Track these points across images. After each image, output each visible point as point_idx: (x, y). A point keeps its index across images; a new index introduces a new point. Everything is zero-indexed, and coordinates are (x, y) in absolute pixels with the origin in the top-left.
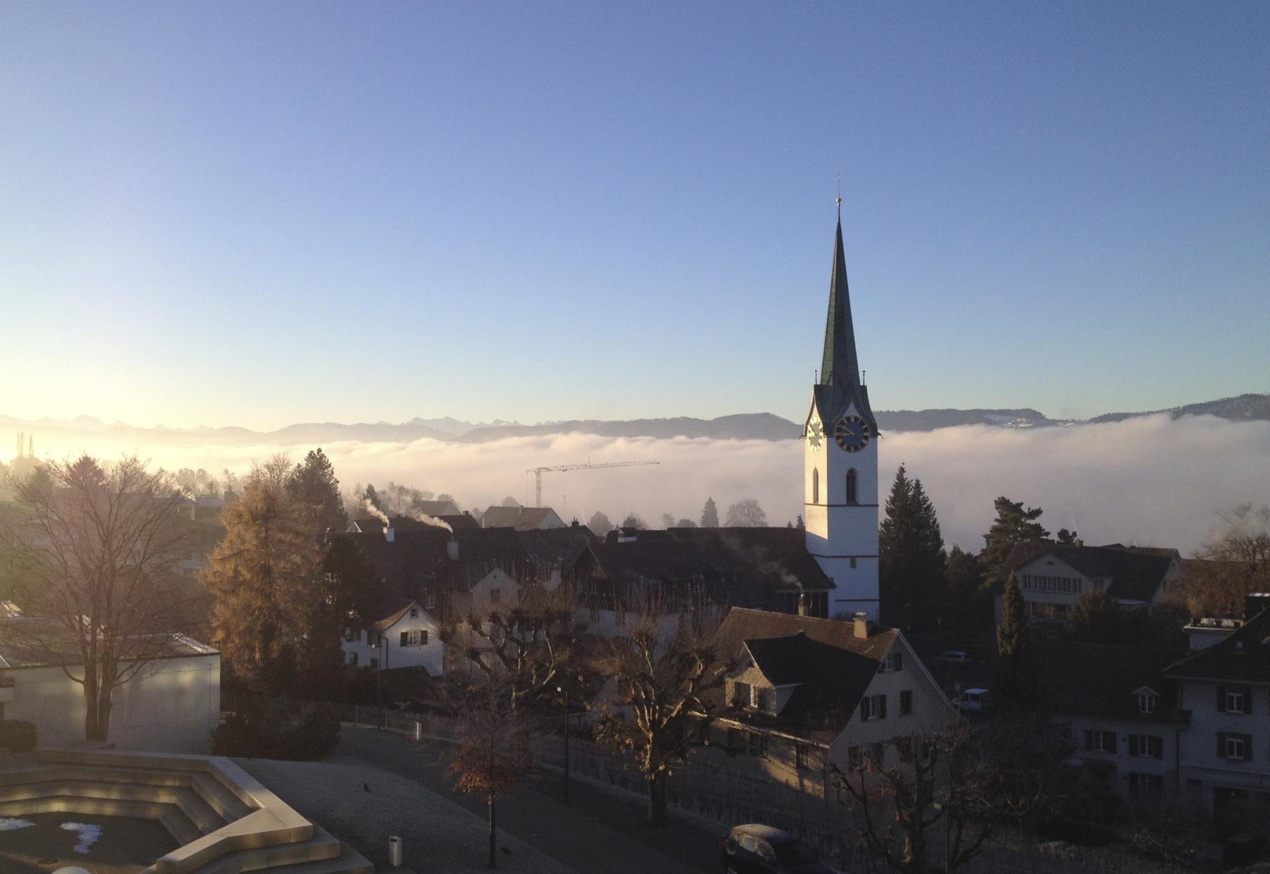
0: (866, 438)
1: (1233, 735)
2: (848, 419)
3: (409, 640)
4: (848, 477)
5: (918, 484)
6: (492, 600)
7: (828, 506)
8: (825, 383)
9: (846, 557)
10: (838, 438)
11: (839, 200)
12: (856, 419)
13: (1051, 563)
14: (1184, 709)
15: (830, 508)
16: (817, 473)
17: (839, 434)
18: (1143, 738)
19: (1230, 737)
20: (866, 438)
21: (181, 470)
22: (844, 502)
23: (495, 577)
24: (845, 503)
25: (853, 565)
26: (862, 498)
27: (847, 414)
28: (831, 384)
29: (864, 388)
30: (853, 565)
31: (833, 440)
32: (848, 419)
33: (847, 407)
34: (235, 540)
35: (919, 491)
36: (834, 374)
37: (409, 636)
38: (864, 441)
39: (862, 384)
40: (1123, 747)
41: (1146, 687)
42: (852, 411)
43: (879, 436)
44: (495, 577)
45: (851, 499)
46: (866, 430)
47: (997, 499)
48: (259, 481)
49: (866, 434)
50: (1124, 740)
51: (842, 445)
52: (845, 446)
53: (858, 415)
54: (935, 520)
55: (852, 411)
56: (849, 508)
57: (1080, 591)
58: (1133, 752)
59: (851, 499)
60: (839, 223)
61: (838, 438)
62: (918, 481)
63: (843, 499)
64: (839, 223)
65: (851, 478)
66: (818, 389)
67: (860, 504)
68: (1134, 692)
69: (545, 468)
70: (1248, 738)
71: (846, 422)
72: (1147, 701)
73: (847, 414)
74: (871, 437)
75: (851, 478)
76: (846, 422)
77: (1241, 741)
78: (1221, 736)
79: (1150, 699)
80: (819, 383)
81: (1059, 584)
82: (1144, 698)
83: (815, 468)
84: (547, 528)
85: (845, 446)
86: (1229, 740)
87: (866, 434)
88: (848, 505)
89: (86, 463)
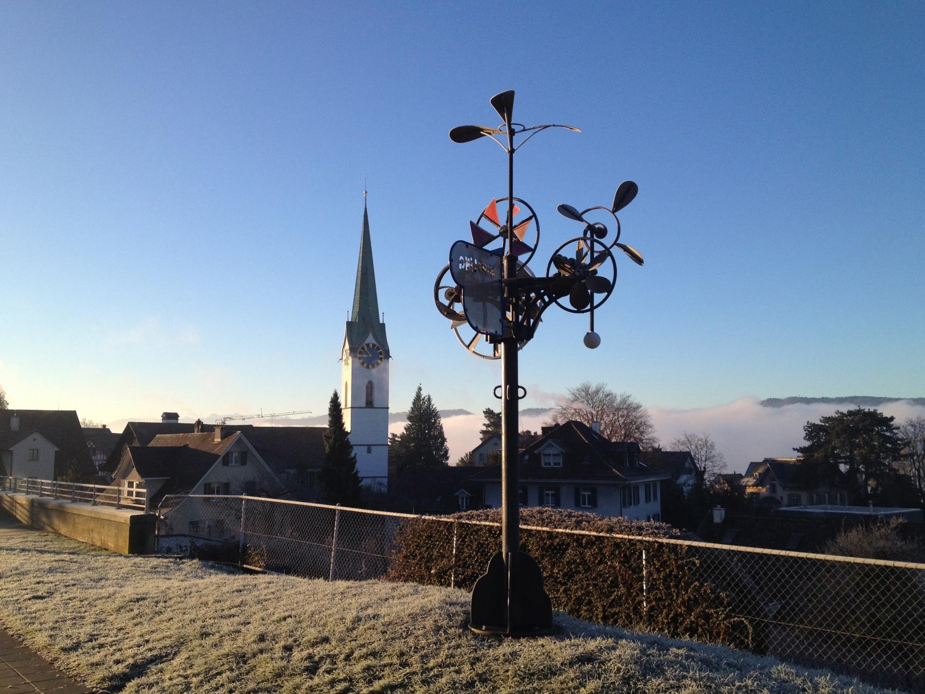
0: (381, 359)
2: (368, 345)
4: (367, 387)
5: (429, 399)
7: (351, 408)
8: (354, 320)
9: (364, 445)
11: (366, 193)
12: (374, 345)
15: (354, 409)
23: (35, 440)
24: (364, 405)
25: (369, 451)
26: (376, 403)
27: (367, 342)
28: (357, 321)
29: (383, 325)
30: (369, 451)
33: (367, 337)
34: (521, 661)
36: (360, 314)
38: (379, 361)
39: (381, 322)
41: (462, 490)
42: (370, 340)
43: (390, 358)
44: (35, 440)
45: (370, 404)
46: (381, 354)
47: (485, 410)
52: (365, 364)
53: (374, 342)
55: (370, 340)
56: (367, 409)
59: (370, 404)
60: (366, 209)
62: (429, 396)
63: (363, 403)
64: (366, 209)
65: (370, 387)
66: (349, 324)
67: (375, 406)
68: (456, 494)
69: (230, 418)
72: (465, 501)
73: (367, 342)
74: (385, 359)
75: (370, 387)
79: (466, 499)
80: (350, 320)
82: (463, 499)
84: (194, 448)
85: (365, 364)
88: (366, 407)
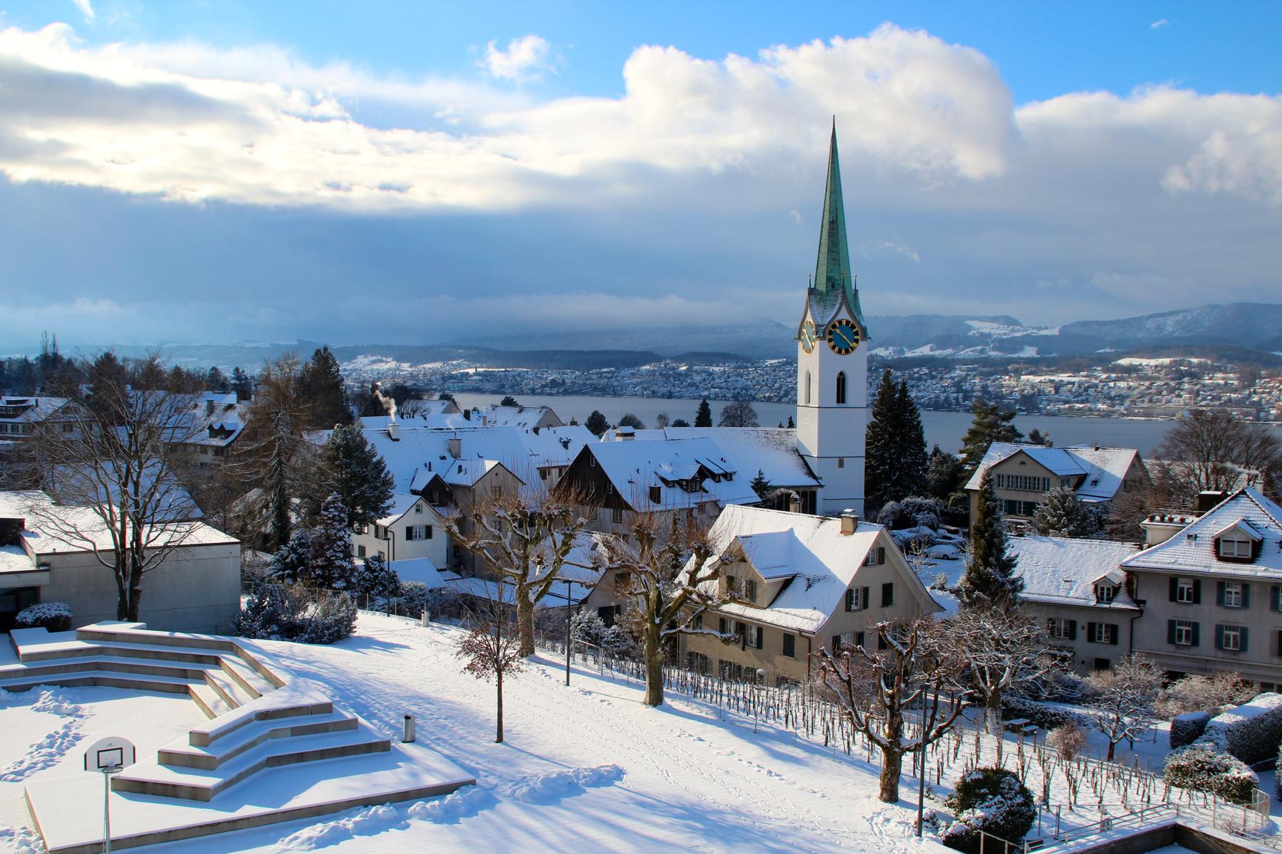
0: (857, 341)
1: (1181, 623)
2: (840, 322)
3: (414, 534)
4: (838, 379)
6: (1097, 597)
10: (830, 340)
12: (848, 322)
13: (1023, 463)
14: (612, 510)
16: (844, 379)
17: (831, 337)
18: (1101, 626)
19: (1179, 625)
20: (857, 341)
21: (868, 427)
22: (835, 404)
25: (841, 464)
30: (841, 464)
31: (826, 342)
32: (840, 322)
35: (906, 394)
37: (414, 531)
40: (1082, 634)
46: (856, 333)
48: (365, 395)
49: (856, 337)
50: (1083, 628)
51: (833, 348)
52: (837, 349)
53: (849, 318)
54: (919, 422)
57: (1048, 489)
58: (1091, 638)
60: (834, 129)
61: (830, 340)
64: (834, 129)
70: (1195, 626)
71: (838, 325)
76: (838, 325)
77: (1237, 633)
78: (1172, 624)
80: (813, 286)
81: (1038, 484)
83: (808, 371)
85: (837, 349)
86: (1226, 632)
87: (856, 337)
89: (10, 358)
